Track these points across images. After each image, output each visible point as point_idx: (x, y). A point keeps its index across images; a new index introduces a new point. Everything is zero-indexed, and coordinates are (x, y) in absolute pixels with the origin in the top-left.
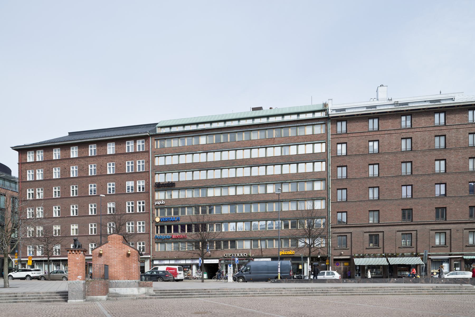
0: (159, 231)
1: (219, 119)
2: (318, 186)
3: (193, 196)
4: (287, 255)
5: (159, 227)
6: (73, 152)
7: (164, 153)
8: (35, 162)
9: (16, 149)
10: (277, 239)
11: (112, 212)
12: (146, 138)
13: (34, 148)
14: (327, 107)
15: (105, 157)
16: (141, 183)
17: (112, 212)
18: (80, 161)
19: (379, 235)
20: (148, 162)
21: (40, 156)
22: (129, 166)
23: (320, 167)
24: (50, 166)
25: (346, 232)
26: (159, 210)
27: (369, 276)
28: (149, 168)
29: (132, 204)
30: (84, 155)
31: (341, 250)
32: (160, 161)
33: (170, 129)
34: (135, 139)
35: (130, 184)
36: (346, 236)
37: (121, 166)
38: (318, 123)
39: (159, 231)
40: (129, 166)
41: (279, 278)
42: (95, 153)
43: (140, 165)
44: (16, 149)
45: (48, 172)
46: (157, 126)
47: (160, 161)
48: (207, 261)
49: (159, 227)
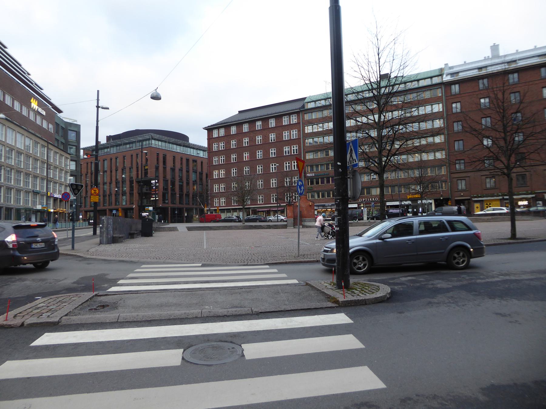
0: (310, 183)
1: (426, 76)
2: (438, 140)
3: (314, 157)
4: (414, 198)
5: (309, 180)
6: (285, 121)
7: (311, 123)
8: (219, 137)
9: (205, 129)
10: (390, 186)
11: (235, 175)
12: (298, 113)
13: (217, 127)
14: (443, 72)
15: (268, 130)
16: (295, 147)
17: (235, 175)
18: (250, 134)
19: (525, 174)
20: (299, 131)
21: (222, 132)
22: (286, 135)
23: (438, 123)
24: (229, 139)
25: (464, 176)
26: (309, 167)
27: (163, 222)
28: (301, 135)
29: (289, 163)
30: (266, 127)
31: (461, 192)
32: (309, 129)
33: (315, 103)
34: (289, 114)
35: (286, 149)
36: (465, 179)
37: (280, 135)
38: (434, 88)
39: (310, 183)
40: (286, 135)
41: (365, 217)
42: (260, 128)
43: (294, 133)
44: (205, 129)
45: (228, 143)
46: (306, 101)
47: (309, 129)
48: (390, 204)
49: (309, 180)
